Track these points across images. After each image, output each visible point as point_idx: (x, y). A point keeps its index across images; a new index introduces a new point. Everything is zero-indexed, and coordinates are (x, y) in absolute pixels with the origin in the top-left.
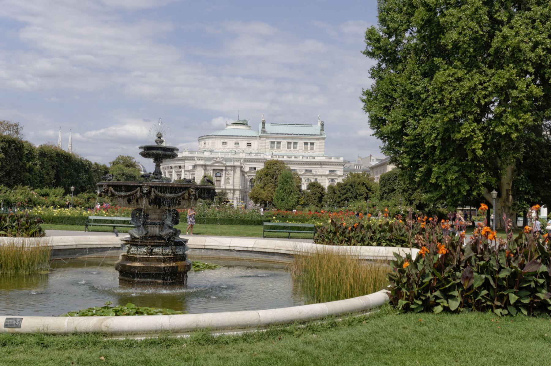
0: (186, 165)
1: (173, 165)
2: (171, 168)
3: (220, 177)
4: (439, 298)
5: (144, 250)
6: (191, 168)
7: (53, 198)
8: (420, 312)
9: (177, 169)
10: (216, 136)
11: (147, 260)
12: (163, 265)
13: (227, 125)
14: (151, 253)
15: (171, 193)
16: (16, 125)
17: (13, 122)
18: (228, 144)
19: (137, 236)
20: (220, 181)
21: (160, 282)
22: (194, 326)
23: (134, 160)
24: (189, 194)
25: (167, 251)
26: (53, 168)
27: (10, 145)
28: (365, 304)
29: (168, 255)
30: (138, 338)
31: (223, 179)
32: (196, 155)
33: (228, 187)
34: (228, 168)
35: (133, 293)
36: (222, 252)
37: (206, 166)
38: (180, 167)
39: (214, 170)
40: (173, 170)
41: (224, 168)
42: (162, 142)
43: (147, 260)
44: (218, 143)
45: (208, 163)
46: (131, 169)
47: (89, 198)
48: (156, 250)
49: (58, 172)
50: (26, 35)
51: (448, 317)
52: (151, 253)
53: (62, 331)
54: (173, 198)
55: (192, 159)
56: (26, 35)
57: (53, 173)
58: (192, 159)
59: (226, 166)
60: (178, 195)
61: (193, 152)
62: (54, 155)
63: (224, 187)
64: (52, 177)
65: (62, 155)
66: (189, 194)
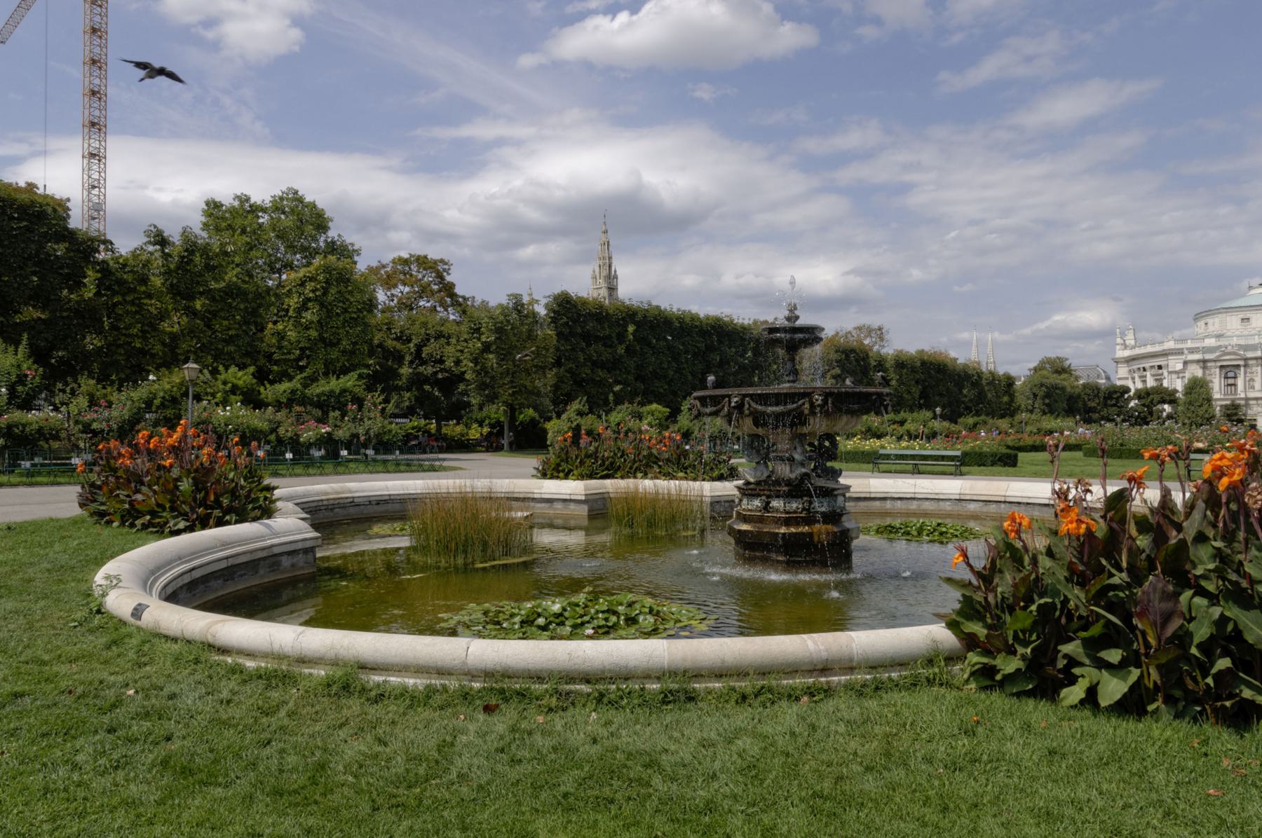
0: (1171, 363)
1: (1147, 365)
2: (1144, 369)
3: (1235, 377)
4: (1081, 664)
5: (757, 503)
6: (1179, 366)
7: (907, 426)
8: (1018, 695)
9: (1155, 371)
10: (1228, 310)
11: (761, 520)
12: (783, 530)
13: (1250, 288)
14: (766, 507)
15: (777, 405)
16: (880, 329)
17: (875, 325)
18: (1253, 320)
19: (752, 480)
20: (1235, 385)
21: (780, 558)
22: (331, 654)
23: (1068, 363)
24: (812, 405)
25: (794, 505)
26: (917, 382)
27: (847, 356)
28: (824, 655)
29: (795, 512)
30: (250, 664)
31: (1240, 382)
32: (1190, 344)
33: (1251, 395)
34: (1251, 362)
35: (714, 575)
36: (1037, 508)
37: (1205, 361)
38: (1160, 367)
39: (1222, 367)
40: (1148, 374)
41: (1242, 363)
42: (797, 318)
43: (761, 520)
44: (1232, 323)
45: (1208, 357)
46: (1064, 376)
47: (975, 425)
48: (775, 503)
49: (924, 388)
50: (916, 200)
51: (1086, 721)
52: (766, 507)
53: (171, 633)
54: (782, 414)
55: (1179, 352)
56: (916, 200)
57: (916, 390)
58: (1179, 352)
59: (1246, 359)
60: (790, 407)
61: (1183, 340)
62: (918, 364)
63: (1243, 395)
64: (917, 396)
65: (931, 363)
66: (812, 405)
